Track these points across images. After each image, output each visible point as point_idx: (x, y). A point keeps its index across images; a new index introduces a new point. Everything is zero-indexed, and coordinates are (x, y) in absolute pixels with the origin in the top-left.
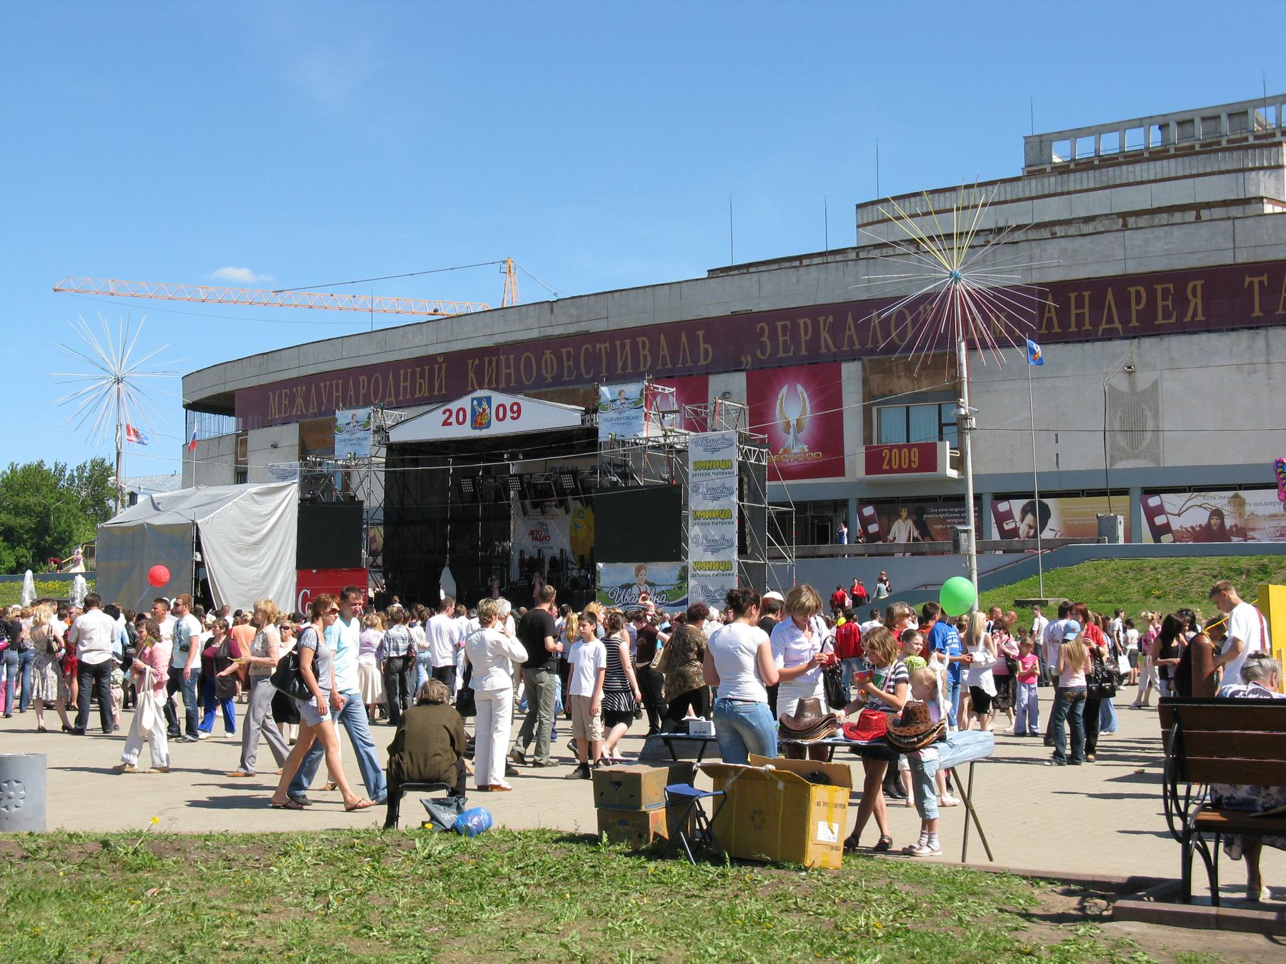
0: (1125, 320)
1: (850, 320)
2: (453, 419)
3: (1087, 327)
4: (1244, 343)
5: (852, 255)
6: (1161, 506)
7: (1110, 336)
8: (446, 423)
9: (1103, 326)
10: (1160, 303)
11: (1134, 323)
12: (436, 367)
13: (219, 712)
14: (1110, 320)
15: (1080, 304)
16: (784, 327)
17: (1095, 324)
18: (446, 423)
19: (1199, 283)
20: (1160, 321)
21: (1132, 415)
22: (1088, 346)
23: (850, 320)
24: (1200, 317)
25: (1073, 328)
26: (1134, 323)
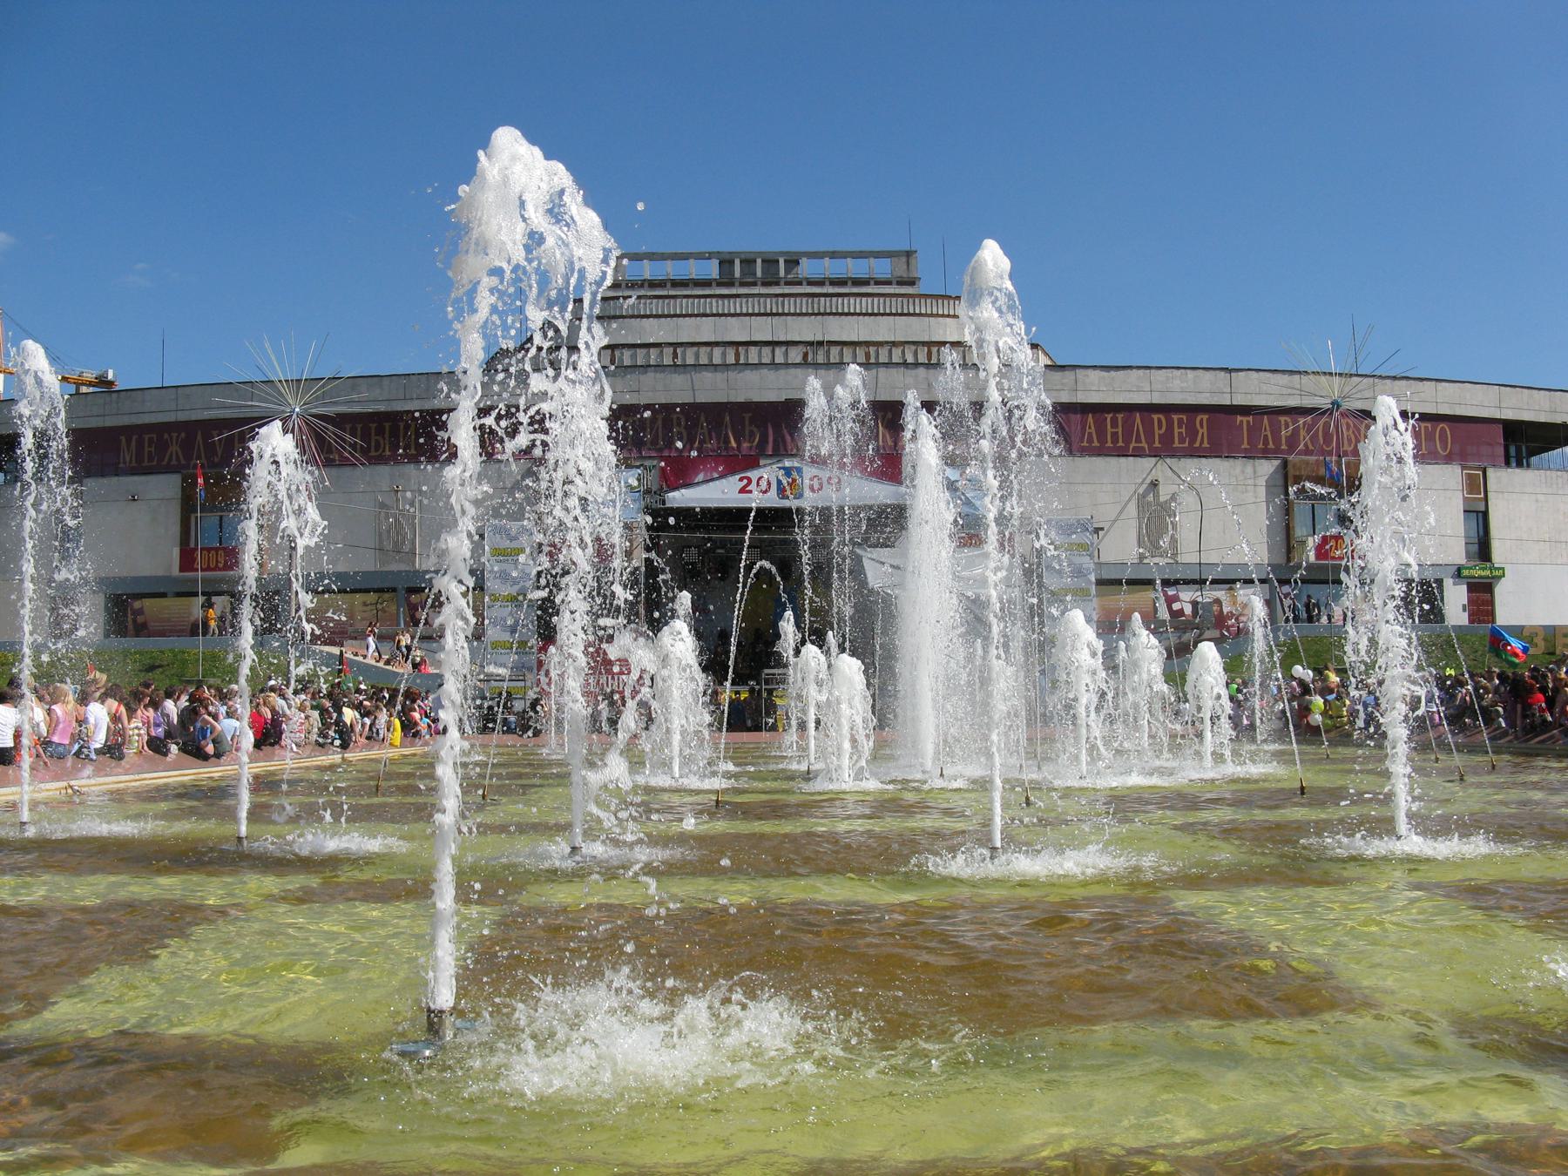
0: (1150, 441)
1: (199, 437)
2: (753, 487)
3: (1120, 444)
4: (1238, 470)
5: (795, 355)
6: (1423, 598)
7: (1138, 453)
8: (742, 491)
9: (1133, 445)
10: (1176, 431)
11: (1157, 444)
12: (402, 425)
13: (1225, 854)
14: (1138, 440)
15: (1114, 425)
16: (151, 440)
17: (1127, 441)
18: (742, 491)
19: (1205, 417)
20: (1176, 444)
21: (1155, 517)
22: (1123, 460)
23: (199, 437)
24: (1206, 445)
25: (1109, 444)
26: (1157, 444)
